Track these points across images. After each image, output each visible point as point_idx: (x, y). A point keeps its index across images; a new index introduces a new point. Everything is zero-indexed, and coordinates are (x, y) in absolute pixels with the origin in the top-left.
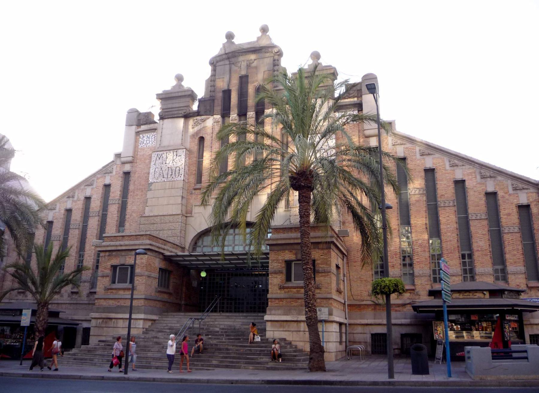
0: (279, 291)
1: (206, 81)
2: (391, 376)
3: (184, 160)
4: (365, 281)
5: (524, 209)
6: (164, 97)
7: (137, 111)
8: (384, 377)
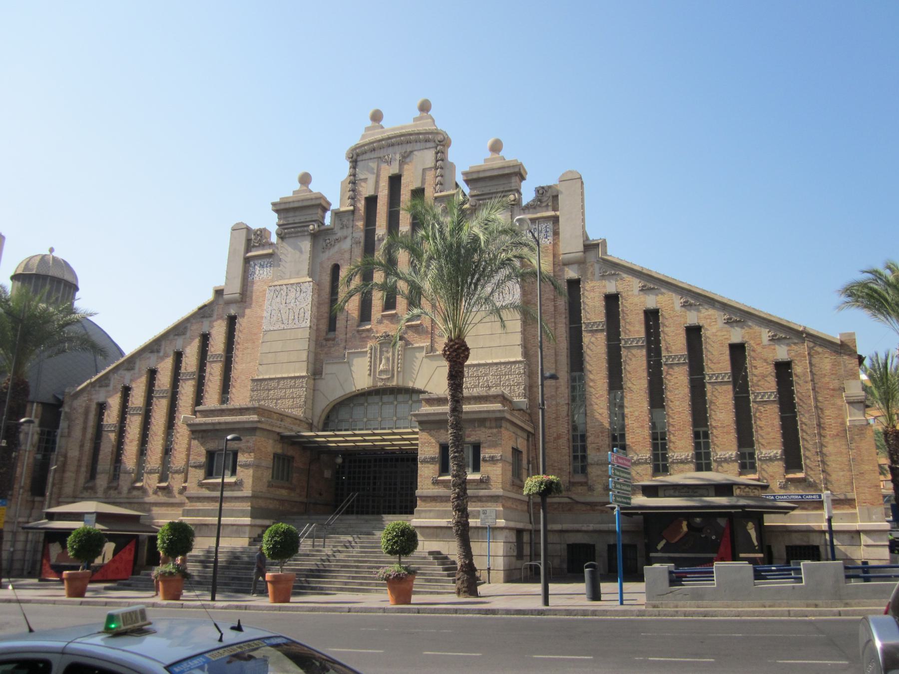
0: (432, 487)
1: (342, 183)
2: (546, 602)
3: (310, 299)
4: (559, 469)
5: (783, 369)
6: (282, 209)
7: (248, 229)
8: (537, 604)
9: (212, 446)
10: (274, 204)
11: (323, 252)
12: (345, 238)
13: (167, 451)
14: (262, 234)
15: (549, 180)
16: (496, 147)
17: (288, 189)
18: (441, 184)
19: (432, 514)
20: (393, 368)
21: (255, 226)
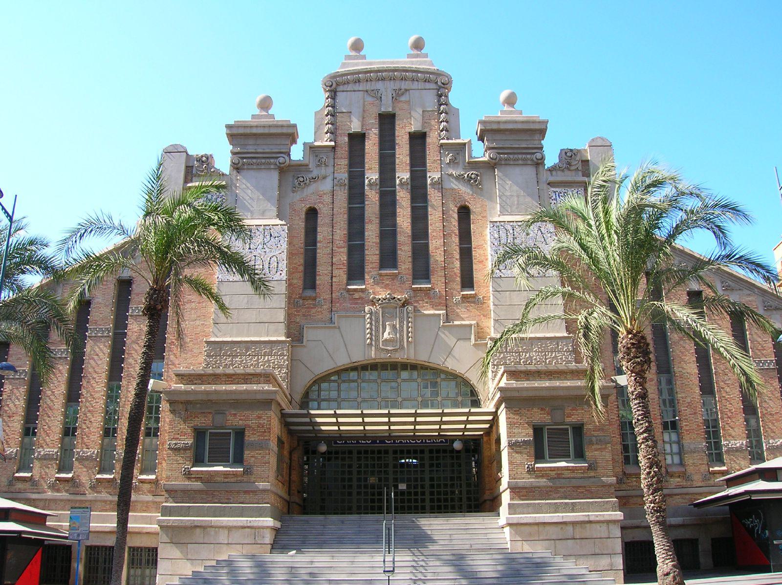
6: (238, 135)
9: (201, 421)
10: (228, 127)
11: (293, 192)
12: (324, 178)
13: (69, 431)
14: (206, 161)
15: (580, 143)
16: (265, 104)
17: (245, 112)
18: (447, 130)
19: (530, 509)
20: (402, 336)
21: (195, 151)
